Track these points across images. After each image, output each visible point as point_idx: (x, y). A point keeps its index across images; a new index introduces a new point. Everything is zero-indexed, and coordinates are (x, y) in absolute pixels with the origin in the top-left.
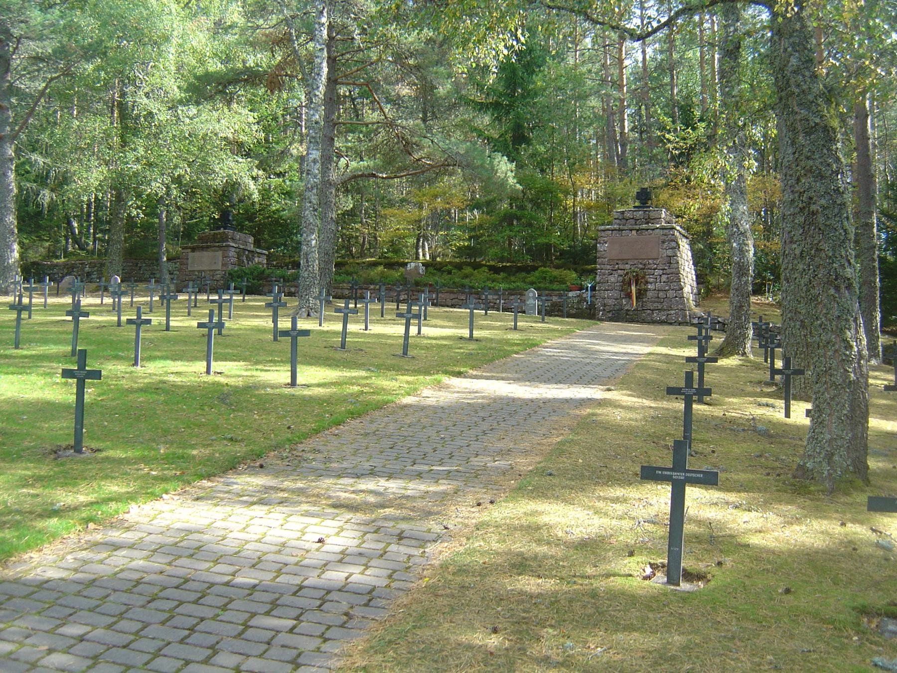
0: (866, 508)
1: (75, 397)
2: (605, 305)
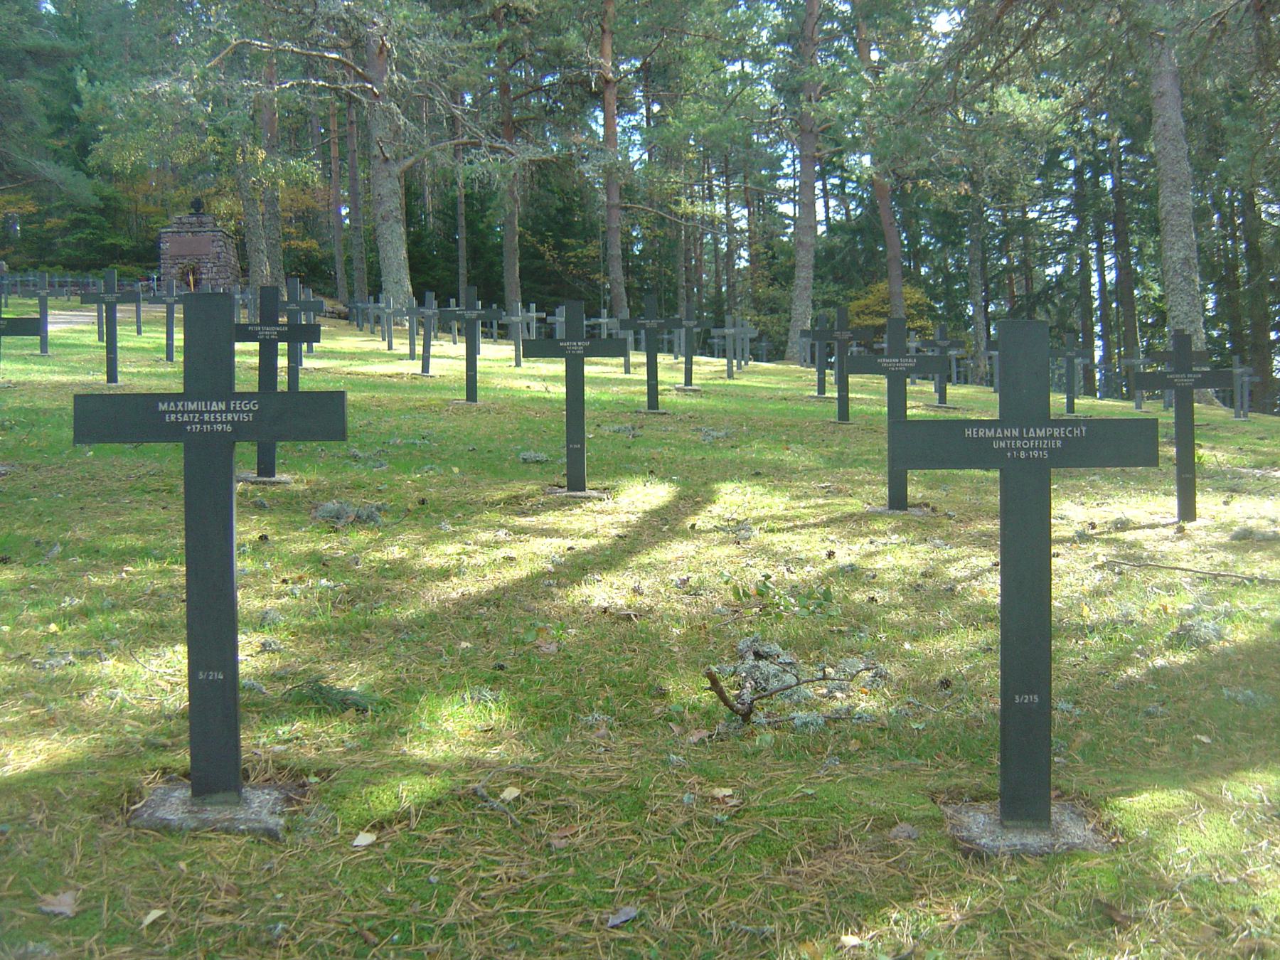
0: (350, 396)
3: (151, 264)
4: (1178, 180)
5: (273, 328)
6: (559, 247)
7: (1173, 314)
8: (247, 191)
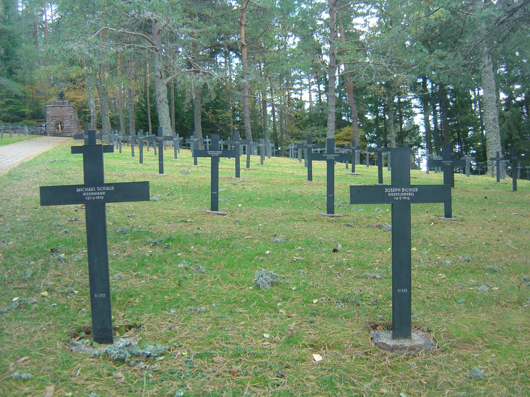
1: (219, 167)
2: (50, 132)
3: (40, 120)
4: (491, 88)
5: (333, 155)
6: (214, 113)
7: (489, 141)
8: (101, 90)
